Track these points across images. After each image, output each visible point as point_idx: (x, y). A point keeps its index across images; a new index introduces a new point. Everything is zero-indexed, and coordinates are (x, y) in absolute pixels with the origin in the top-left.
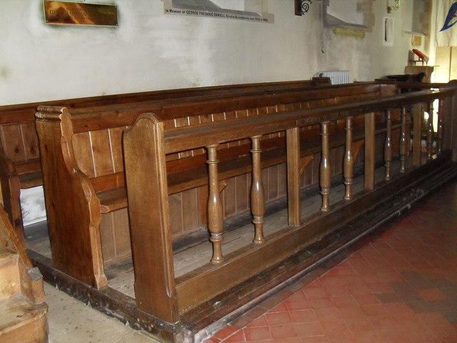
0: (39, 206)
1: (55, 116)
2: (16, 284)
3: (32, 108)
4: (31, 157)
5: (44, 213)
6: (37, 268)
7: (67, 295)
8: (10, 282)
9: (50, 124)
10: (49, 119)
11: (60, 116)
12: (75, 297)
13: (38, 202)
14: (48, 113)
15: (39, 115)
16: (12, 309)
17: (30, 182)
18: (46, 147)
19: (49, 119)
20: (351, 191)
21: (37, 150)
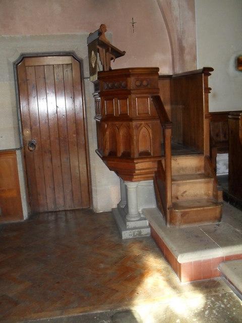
0: (225, 166)
1: (237, 117)
2: (211, 192)
3: (227, 113)
4: (224, 139)
5: (227, 171)
6: (209, 87)
7: (233, 207)
8: (208, 190)
9: (234, 121)
10: (234, 119)
11: (240, 117)
12: (237, 207)
13: (225, 164)
14: (234, 115)
15: (230, 116)
16: (208, 202)
17: (222, 151)
18: (232, 132)
19: (234, 119)
20: (227, 259)
21: (227, 136)
